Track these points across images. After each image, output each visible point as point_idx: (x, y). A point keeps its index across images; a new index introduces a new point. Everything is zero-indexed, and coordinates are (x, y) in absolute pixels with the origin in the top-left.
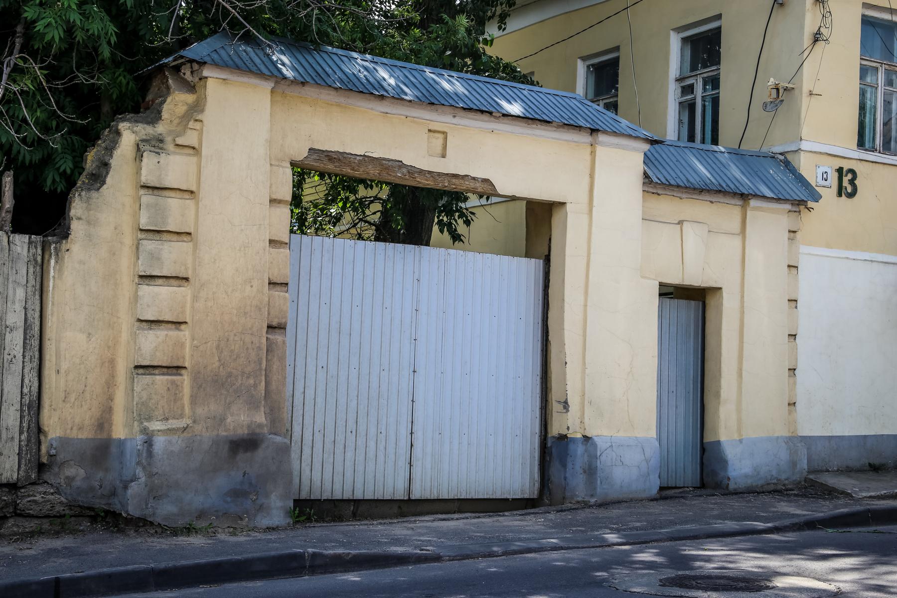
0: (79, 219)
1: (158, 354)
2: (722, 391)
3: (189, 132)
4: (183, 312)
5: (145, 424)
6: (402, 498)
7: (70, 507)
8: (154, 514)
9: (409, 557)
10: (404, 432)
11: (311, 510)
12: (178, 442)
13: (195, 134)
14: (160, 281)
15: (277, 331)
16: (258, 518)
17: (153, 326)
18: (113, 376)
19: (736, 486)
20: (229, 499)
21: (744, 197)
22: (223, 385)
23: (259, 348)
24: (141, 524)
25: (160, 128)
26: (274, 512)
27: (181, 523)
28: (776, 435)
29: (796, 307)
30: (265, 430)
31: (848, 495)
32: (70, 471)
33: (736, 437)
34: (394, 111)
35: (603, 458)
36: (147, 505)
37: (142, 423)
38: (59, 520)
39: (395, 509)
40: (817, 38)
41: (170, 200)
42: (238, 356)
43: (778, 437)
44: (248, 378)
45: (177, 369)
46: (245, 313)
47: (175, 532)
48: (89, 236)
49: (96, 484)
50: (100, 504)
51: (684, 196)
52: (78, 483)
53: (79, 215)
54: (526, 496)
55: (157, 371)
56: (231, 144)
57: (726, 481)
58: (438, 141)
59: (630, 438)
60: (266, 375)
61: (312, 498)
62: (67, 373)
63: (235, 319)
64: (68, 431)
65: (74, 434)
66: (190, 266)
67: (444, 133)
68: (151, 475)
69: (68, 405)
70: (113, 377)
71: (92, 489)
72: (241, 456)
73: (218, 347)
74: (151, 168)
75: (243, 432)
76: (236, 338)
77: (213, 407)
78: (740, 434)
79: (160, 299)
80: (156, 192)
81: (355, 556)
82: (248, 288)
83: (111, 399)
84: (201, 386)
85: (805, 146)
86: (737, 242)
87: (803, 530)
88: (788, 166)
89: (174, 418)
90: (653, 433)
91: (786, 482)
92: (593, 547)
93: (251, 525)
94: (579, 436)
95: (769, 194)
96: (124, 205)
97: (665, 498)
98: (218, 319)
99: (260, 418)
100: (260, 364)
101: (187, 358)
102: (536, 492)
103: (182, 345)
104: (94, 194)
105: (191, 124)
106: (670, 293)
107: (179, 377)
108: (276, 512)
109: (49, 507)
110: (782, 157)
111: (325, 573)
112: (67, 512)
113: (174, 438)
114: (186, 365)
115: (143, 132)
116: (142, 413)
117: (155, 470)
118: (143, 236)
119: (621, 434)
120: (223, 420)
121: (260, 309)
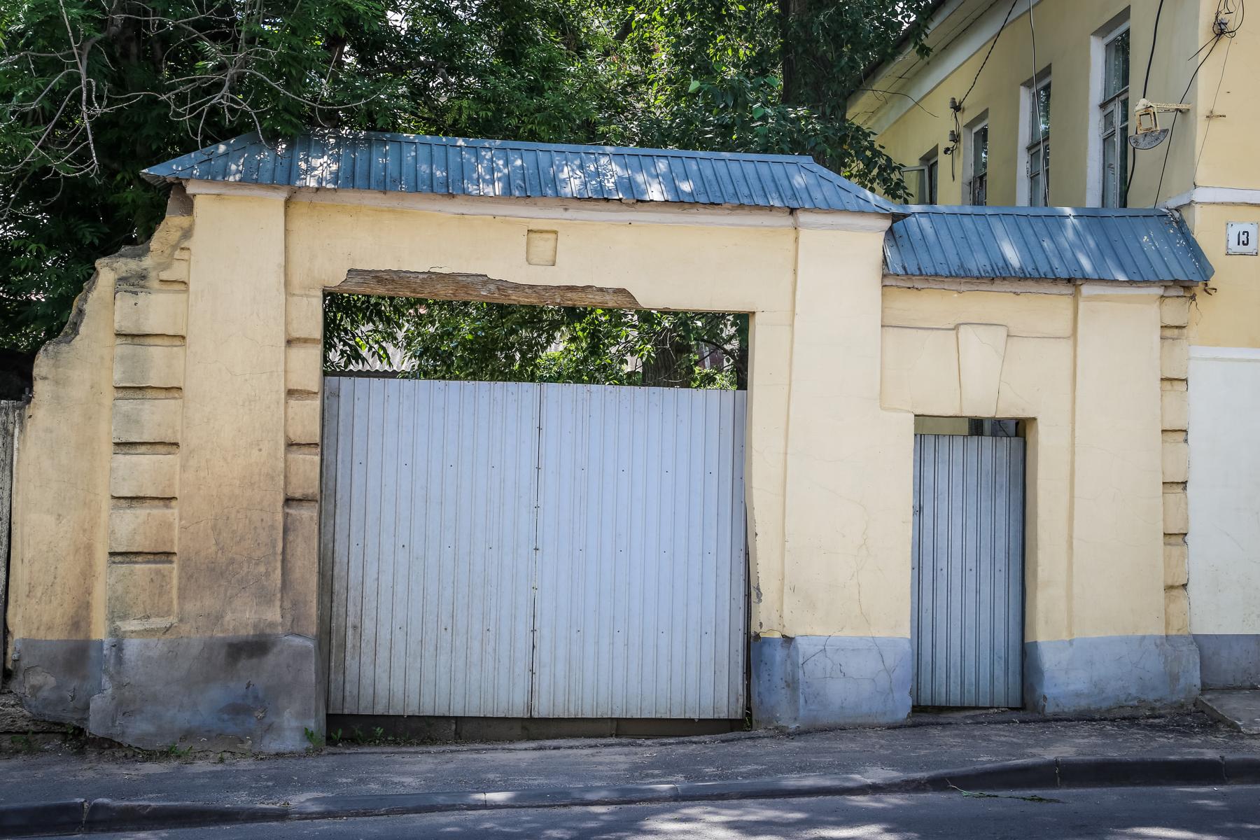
0: (45, 378)
1: (138, 538)
2: (1040, 569)
3: (176, 264)
4: (171, 485)
5: (118, 623)
6: (520, 716)
7: (35, 722)
8: (123, 733)
9: (238, 813)
10: (522, 629)
11: (350, 729)
12: (157, 646)
13: (184, 264)
14: (143, 449)
15: (304, 504)
16: (266, 741)
17: (134, 502)
18: (90, 565)
19: (1057, 710)
20: (226, 717)
21: (1073, 281)
22: (222, 574)
23: (272, 527)
24: (107, 745)
25: (147, 262)
26: (287, 733)
27: (159, 745)
28: (1140, 633)
29: (1186, 441)
30: (280, 630)
31: (1233, 727)
32: (35, 679)
33: (1065, 636)
34: (472, 212)
35: (809, 666)
36: (114, 722)
37: (114, 622)
38: (24, 737)
39: (517, 730)
40: (1221, 30)
41: (151, 348)
42: (242, 538)
43: (1144, 638)
44: (257, 564)
45: (168, 555)
46: (252, 484)
47: (150, 756)
48: (57, 398)
49: (68, 695)
50: (71, 719)
51: (963, 288)
52: (45, 693)
53: (43, 374)
54: (723, 715)
55: (140, 559)
56: (235, 276)
57: (1042, 702)
58: (543, 246)
59: (861, 638)
60: (283, 561)
61: (391, 713)
62: (31, 563)
63: (237, 491)
64: (34, 632)
65: (41, 635)
66: (178, 428)
67: (555, 232)
68: (120, 686)
69: (34, 601)
70: (91, 566)
71: (62, 700)
72: (244, 663)
73: (214, 528)
74: (125, 312)
75: (247, 632)
76: (240, 516)
77: (210, 602)
78: (1071, 634)
79: (142, 471)
80: (137, 340)
81: (155, 810)
82: (255, 452)
83: (89, 592)
84: (191, 576)
85: (1199, 195)
86: (1065, 347)
87: (924, 791)
88: (1182, 228)
89: (158, 616)
90: (905, 632)
91: (1158, 704)
92: (539, 807)
93: (256, 750)
94: (777, 635)
95: (1121, 277)
96: (102, 358)
97: (915, 726)
98: (214, 493)
99: (273, 614)
100: (274, 547)
101: (176, 542)
102: (740, 711)
103: (170, 526)
104: (64, 347)
105: (178, 254)
106: (929, 431)
107: (167, 566)
108: (292, 726)
109: (9, 721)
110: (1177, 215)
111: (109, 830)
112: (32, 728)
113: (152, 641)
114: (176, 550)
115: (124, 268)
116: (118, 612)
117: (126, 680)
118: (120, 395)
119: (848, 633)
120: (219, 617)
121: (272, 478)
